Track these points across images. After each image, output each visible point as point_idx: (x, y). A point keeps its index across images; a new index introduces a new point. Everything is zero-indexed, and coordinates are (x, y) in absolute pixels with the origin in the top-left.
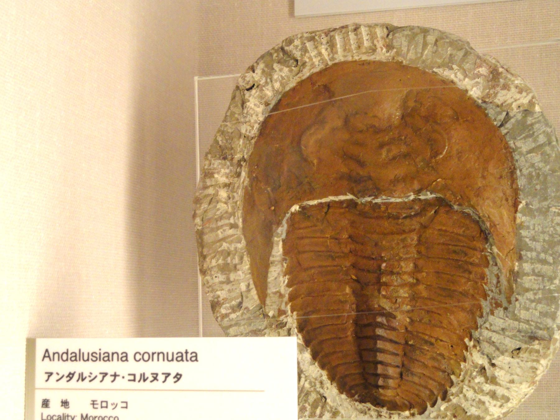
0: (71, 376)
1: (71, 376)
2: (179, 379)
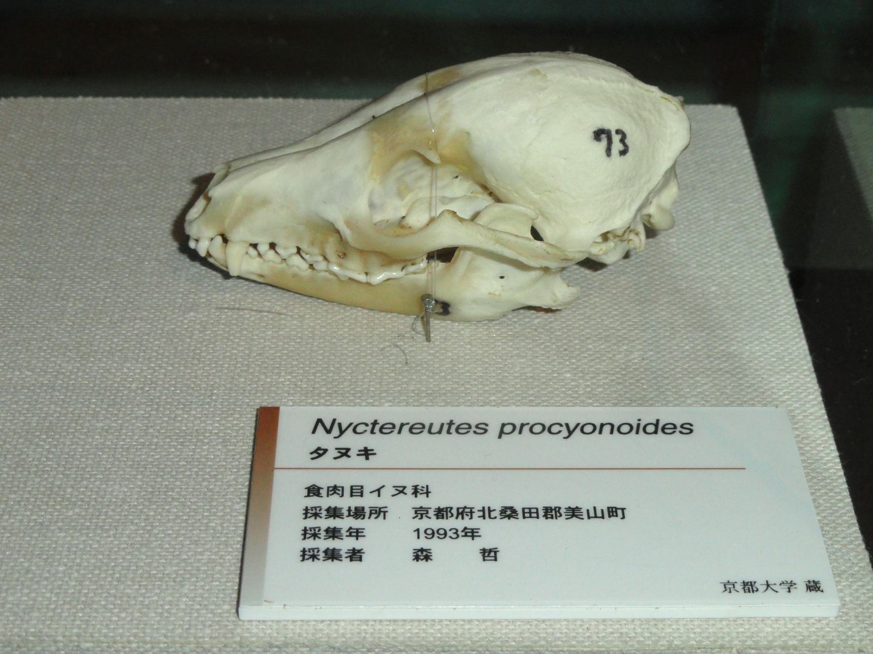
0: (321, 452)
1: (321, 452)
2: (320, 455)
